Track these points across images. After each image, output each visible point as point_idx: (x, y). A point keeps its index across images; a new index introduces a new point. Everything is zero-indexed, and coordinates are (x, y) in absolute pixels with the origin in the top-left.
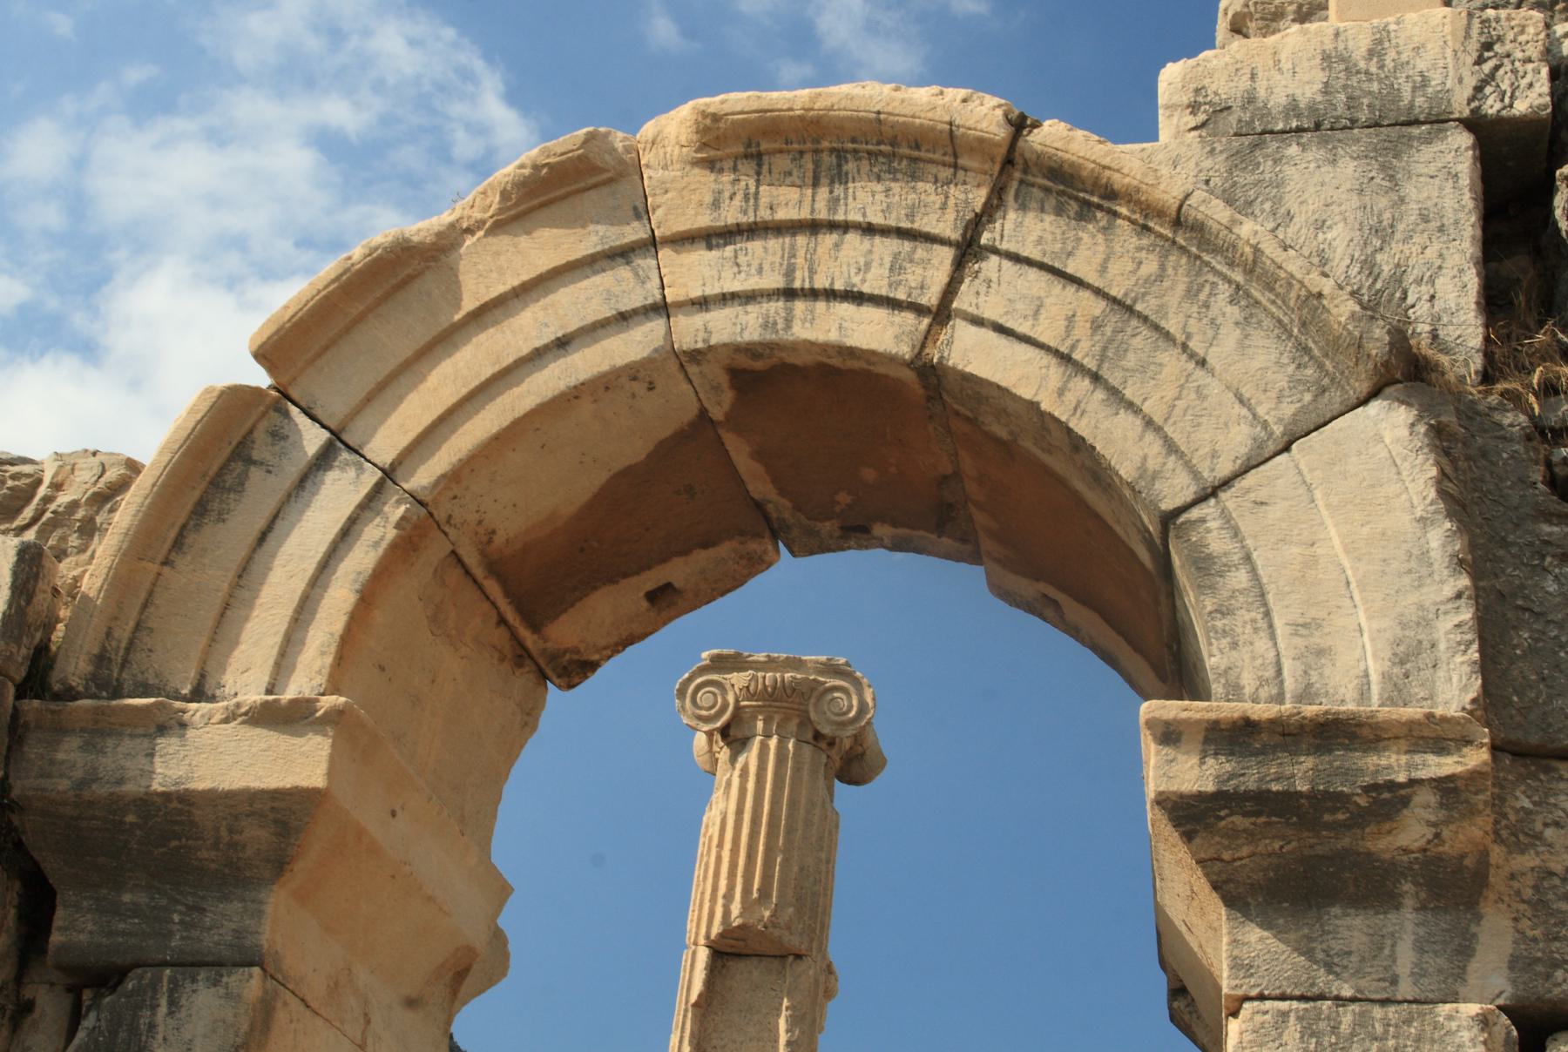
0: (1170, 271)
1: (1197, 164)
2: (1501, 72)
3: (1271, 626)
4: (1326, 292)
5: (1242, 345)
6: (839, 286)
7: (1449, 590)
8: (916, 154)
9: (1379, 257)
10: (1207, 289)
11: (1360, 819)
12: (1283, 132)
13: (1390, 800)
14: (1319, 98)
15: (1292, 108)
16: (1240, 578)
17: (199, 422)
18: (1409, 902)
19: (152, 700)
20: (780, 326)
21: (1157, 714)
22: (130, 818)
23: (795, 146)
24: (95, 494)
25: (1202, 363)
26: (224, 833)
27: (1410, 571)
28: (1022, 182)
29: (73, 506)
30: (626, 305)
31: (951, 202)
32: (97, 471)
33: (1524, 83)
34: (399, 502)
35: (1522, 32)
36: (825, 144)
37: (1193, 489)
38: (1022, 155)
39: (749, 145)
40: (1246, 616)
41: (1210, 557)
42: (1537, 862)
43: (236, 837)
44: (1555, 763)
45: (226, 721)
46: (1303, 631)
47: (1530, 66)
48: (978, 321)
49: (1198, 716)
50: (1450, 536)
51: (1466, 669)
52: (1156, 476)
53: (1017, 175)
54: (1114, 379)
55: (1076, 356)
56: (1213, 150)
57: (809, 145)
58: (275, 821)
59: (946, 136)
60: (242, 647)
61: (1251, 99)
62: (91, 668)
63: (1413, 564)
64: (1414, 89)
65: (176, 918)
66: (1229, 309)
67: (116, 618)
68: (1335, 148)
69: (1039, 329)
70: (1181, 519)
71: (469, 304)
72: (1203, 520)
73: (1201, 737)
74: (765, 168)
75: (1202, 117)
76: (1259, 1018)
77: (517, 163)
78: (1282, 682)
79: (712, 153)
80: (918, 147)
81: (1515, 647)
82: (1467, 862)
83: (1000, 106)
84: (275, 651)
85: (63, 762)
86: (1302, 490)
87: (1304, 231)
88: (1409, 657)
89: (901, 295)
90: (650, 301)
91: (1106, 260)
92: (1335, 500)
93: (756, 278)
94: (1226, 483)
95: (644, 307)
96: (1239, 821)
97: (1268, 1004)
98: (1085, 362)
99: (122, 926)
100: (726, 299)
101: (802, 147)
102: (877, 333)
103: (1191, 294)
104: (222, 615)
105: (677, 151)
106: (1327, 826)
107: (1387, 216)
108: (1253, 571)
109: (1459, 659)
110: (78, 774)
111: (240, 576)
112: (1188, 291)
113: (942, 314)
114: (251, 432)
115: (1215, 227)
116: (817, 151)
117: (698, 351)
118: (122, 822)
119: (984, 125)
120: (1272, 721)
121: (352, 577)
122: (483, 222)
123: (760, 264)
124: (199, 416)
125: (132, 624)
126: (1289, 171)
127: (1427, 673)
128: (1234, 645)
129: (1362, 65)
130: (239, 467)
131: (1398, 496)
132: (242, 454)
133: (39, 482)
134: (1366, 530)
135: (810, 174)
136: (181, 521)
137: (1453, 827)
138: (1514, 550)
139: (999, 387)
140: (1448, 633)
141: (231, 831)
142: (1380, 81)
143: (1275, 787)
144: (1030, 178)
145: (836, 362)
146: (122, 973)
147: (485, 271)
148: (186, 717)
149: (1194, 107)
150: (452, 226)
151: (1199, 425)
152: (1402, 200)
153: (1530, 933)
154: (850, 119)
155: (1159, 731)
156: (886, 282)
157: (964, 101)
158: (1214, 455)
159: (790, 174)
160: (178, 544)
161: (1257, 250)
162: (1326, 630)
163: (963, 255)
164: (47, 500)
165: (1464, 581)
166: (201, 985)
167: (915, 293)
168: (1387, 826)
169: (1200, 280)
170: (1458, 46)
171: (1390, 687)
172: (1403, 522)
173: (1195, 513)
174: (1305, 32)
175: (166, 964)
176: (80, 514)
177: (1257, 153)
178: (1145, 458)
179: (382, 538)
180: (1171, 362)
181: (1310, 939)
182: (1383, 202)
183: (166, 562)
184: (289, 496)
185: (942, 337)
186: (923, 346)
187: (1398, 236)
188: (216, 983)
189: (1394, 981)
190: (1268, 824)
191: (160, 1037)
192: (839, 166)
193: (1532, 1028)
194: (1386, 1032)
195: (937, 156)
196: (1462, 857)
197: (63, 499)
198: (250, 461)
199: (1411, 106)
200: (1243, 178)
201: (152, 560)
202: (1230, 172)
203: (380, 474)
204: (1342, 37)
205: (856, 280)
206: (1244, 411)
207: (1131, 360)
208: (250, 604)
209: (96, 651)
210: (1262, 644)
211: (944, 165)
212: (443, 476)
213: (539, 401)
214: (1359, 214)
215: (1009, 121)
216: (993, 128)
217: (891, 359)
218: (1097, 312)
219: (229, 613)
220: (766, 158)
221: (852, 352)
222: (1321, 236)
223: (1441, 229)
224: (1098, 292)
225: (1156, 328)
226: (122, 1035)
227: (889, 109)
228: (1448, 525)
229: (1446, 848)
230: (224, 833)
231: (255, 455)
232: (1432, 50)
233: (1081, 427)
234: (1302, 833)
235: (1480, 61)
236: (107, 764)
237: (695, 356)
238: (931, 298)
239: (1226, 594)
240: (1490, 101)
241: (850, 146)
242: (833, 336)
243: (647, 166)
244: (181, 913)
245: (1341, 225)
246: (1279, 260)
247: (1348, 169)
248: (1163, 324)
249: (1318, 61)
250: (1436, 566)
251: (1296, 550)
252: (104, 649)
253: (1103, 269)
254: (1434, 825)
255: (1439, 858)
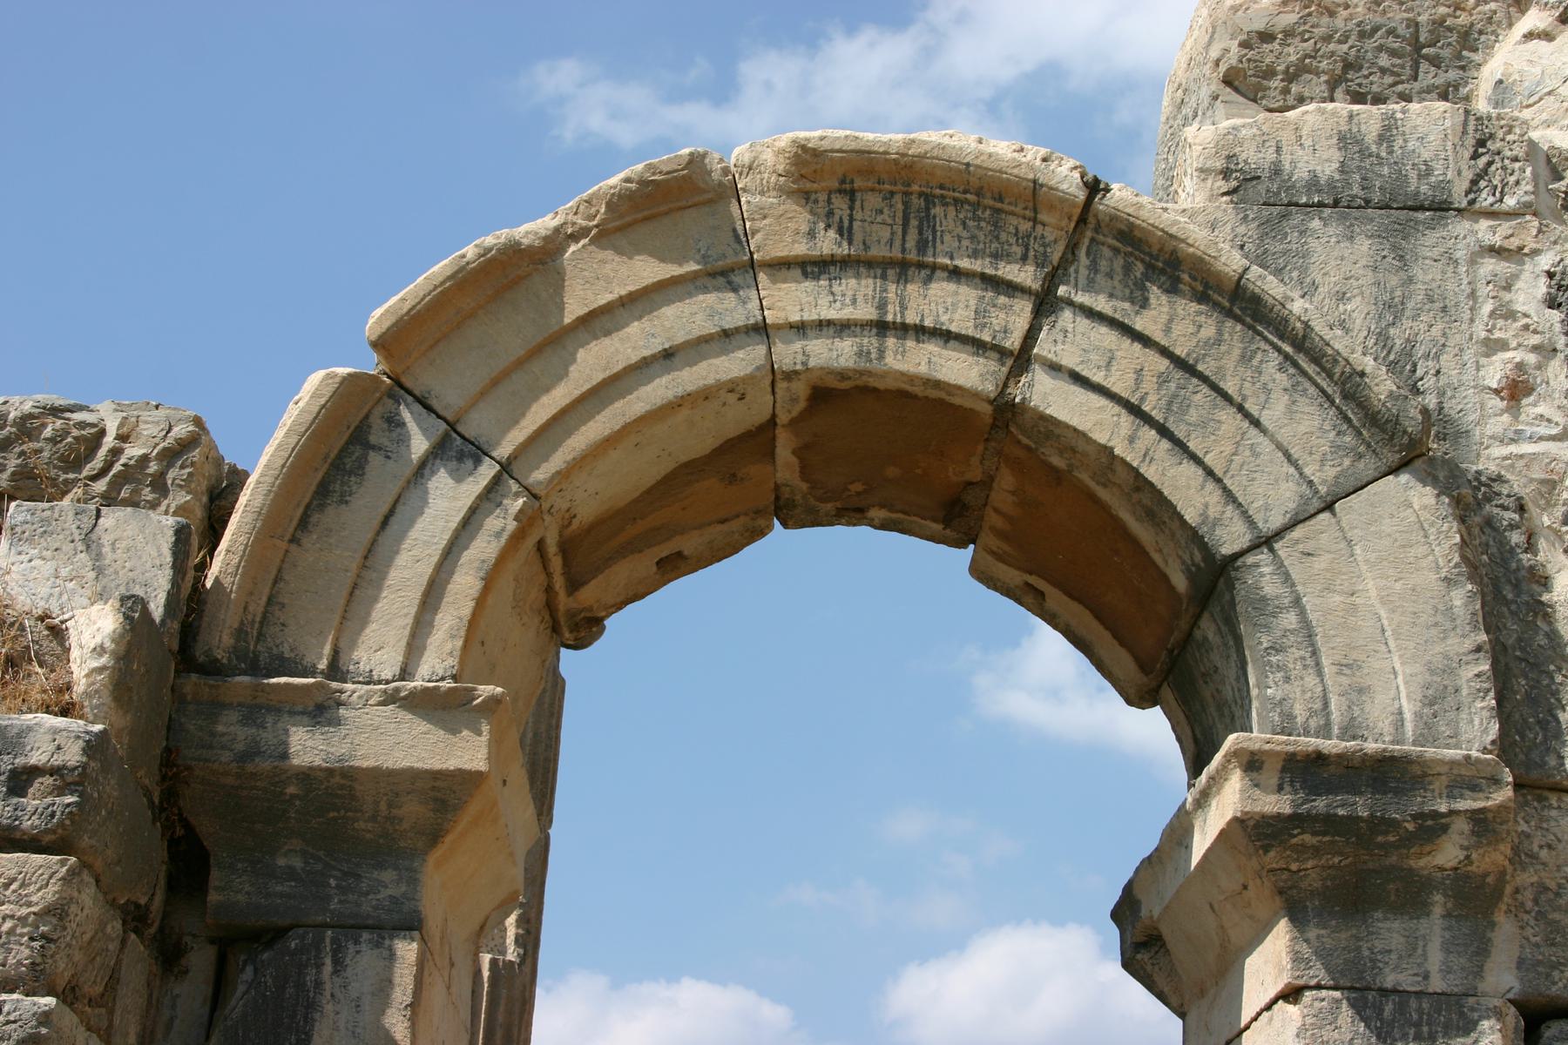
0: (1226, 336)
1: (1233, 230)
2: (1493, 168)
3: (1318, 664)
4: (1368, 370)
5: (1290, 411)
6: (928, 323)
7: (1469, 644)
8: (999, 205)
9: (1392, 331)
10: (1259, 356)
11: (1408, 840)
12: (1306, 205)
13: (1432, 828)
14: (1337, 177)
15: (1313, 183)
16: (1290, 620)
17: (323, 406)
18: (1438, 911)
19: (312, 680)
20: (873, 356)
21: (1245, 745)
22: (291, 790)
23: (887, 187)
24: (165, 449)
25: (1256, 423)
26: (383, 806)
27: (1436, 624)
28: (1093, 240)
29: (144, 459)
30: (728, 324)
31: (1032, 253)
32: (165, 426)
33: (1512, 179)
34: (517, 495)
35: (1509, 132)
36: (915, 188)
37: (1248, 537)
38: (1096, 216)
39: (843, 182)
40: (1294, 655)
41: (1264, 599)
42: (1535, 879)
43: (394, 811)
44: (1546, 793)
45: (383, 703)
46: (1348, 672)
47: (1517, 165)
48: (1054, 368)
49: (1278, 748)
50: (1471, 596)
51: (1486, 714)
52: (1216, 522)
53: (1089, 234)
54: (1180, 432)
55: (1146, 408)
56: (1246, 217)
57: (900, 187)
58: (436, 800)
59: (1029, 192)
60: (373, 626)
61: (1277, 171)
62: (232, 641)
63: (1439, 618)
64: (1420, 177)
65: (333, 882)
66: (1278, 376)
67: (251, 594)
68: (1352, 225)
69: (1112, 380)
70: (1239, 563)
71: (573, 309)
72: (1257, 565)
73: (1279, 766)
74: (858, 204)
75: (1234, 184)
76: (1317, 1004)
77: (622, 175)
78: (1328, 715)
79: (809, 186)
80: (1001, 199)
81: (1516, 693)
82: (1489, 880)
83: (1076, 168)
84: (407, 632)
85: (223, 735)
86: (1343, 545)
87: (1327, 301)
88: (1437, 700)
89: (986, 337)
90: (752, 321)
91: (1171, 321)
92: (1372, 557)
93: (851, 309)
94: (1279, 534)
95: (746, 326)
96: (1308, 838)
97: (1324, 993)
98: (1153, 413)
99: (279, 888)
100: (822, 325)
101: (894, 188)
102: (965, 372)
103: (1245, 359)
104: (351, 594)
105: (773, 179)
106: (1381, 846)
107: (1398, 293)
108: (1302, 613)
109: (1479, 705)
110: (240, 747)
111: (366, 558)
112: (1243, 356)
113: (1021, 360)
114: (367, 417)
115: (1271, 301)
116: (906, 194)
117: (796, 372)
118: (282, 793)
119: (1064, 187)
120: (1339, 756)
121: (476, 564)
122: (589, 230)
123: (853, 298)
124: (323, 401)
125: (265, 599)
126: (1313, 243)
127: (1452, 715)
128: (1287, 679)
129: (1374, 148)
130: (358, 451)
131: (1426, 556)
132: (359, 438)
133: (103, 432)
134: (1398, 586)
135: (900, 214)
136: (307, 500)
137: (1481, 851)
138: (1513, 607)
139: (1075, 430)
140: (1468, 681)
141: (390, 806)
142: (1389, 165)
143: (1341, 812)
144: (1101, 237)
145: (917, 390)
146: (280, 933)
147: (593, 280)
148: (344, 697)
149: (1226, 174)
150: (557, 230)
151: (1253, 480)
152: (1410, 280)
153: (1533, 940)
154: (942, 168)
155: (1245, 759)
156: (971, 324)
157: (1044, 160)
158: (1267, 508)
159: (881, 212)
160: (304, 523)
161: (1306, 325)
162: (1366, 671)
163: (1041, 304)
164: (116, 453)
165: (1483, 637)
166: (364, 947)
167: (1000, 336)
168: (1428, 848)
169: (1254, 347)
170: (1456, 140)
171: (1421, 725)
172: (1429, 579)
173: (1250, 559)
174: (1322, 112)
175: (327, 926)
176: (153, 467)
177: (1285, 223)
178: (1206, 506)
179: (503, 530)
180: (1229, 419)
181: (1359, 939)
182: (1394, 281)
183: (294, 540)
184: (409, 482)
185: (1023, 380)
186: (1005, 385)
187: (1408, 313)
188: (378, 945)
189: (1426, 977)
190: (1332, 842)
191: (327, 994)
192: (928, 209)
193: (1534, 1017)
194: (1421, 1018)
195: (1018, 210)
196: (1486, 875)
197: (133, 451)
198: (369, 446)
199: (1417, 193)
200: (1275, 247)
201: (281, 538)
202: (1261, 238)
203: (498, 467)
204: (1355, 120)
205: (944, 318)
206: (1292, 470)
207: (1193, 415)
208: (378, 585)
209: (236, 625)
210: (1311, 680)
211: (1024, 218)
212: (558, 473)
213: (648, 408)
214: (1375, 289)
215: (1086, 184)
216: (1072, 190)
217: (975, 395)
218: (1162, 369)
219: (357, 592)
220: (858, 195)
221: (938, 384)
222: (1341, 307)
223: (1444, 309)
224: (1165, 352)
225: (1215, 388)
226: (290, 991)
227: (978, 162)
228: (1470, 587)
229: (1473, 868)
230: (383, 806)
231: (373, 439)
232: (1434, 138)
233: (1150, 473)
234: (1344, 845)
235: (1475, 156)
236: (267, 737)
237: (790, 376)
238: (1013, 342)
239: (1279, 634)
240: (1484, 195)
241: (938, 192)
242: (923, 369)
243: (744, 190)
244: (336, 878)
245: (1359, 299)
246: (1327, 338)
247: (1364, 246)
248: (1222, 385)
249: (1335, 141)
250: (1458, 622)
251: (1338, 598)
252: (242, 623)
253: (1167, 330)
254: (1467, 849)
255: (1467, 876)
